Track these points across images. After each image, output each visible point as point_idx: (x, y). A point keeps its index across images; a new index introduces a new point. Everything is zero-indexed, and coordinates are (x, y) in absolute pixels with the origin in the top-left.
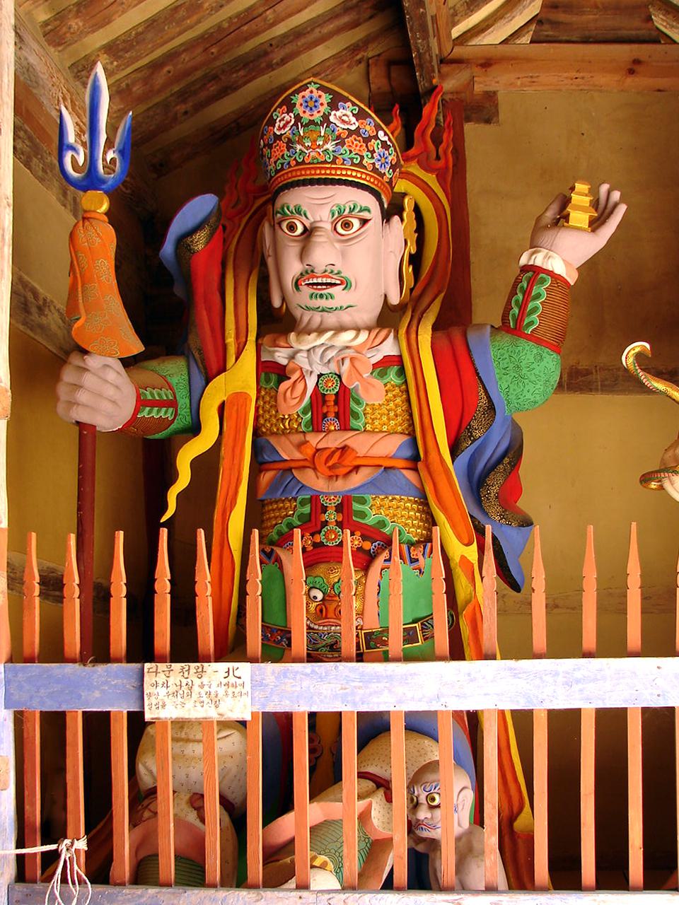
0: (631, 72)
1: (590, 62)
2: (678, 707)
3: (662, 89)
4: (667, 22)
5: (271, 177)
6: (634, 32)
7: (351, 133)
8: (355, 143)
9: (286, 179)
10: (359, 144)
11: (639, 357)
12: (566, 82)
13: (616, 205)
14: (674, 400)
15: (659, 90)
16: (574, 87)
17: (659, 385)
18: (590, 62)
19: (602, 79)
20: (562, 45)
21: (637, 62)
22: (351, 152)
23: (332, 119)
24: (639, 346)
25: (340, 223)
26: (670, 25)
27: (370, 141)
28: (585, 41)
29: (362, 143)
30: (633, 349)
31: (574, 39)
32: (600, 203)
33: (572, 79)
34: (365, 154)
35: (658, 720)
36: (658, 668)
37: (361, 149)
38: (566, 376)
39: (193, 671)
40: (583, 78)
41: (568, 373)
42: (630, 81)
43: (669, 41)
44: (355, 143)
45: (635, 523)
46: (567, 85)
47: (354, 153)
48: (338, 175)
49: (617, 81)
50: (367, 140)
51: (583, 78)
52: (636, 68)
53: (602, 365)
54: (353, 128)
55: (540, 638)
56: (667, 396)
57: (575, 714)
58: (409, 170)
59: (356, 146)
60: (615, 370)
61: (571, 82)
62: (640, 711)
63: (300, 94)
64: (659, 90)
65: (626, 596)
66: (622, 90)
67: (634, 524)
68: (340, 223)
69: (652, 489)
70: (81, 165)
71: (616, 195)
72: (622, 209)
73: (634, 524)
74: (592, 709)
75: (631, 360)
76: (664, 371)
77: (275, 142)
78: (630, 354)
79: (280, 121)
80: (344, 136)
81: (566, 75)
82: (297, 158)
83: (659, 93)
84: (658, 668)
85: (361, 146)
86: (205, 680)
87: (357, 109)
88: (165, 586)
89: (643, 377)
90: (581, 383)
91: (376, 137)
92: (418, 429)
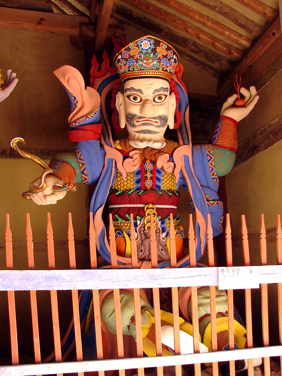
0: (39, 23)
1: (20, 17)
2: (281, 283)
3: (54, 32)
4: (60, 4)
5: (125, 72)
6: (42, 7)
11: (19, 143)
12: (10, 25)
13: (14, 79)
14: (36, 162)
15: (53, 33)
16: (13, 28)
17: (29, 156)
18: (20, 17)
19: (26, 25)
20: (8, 9)
21: (42, 19)
24: (18, 139)
26: (62, 6)
27: (171, 60)
28: (19, 8)
29: (167, 61)
30: (15, 140)
31: (14, 6)
32: (8, 77)
33: (12, 24)
35: (273, 288)
37: (167, 63)
38: (8, 151)
40: (17, 24)
41: (9, 150)
42: (39, 27)
43: (64, 13)
46: (10, 26)
47: (164, 66)
48: (153, 74)
49: (33, 27)
50: (169, 60)
51: (17, 24)
52: (42, 22)
53: (25, 147)
55: (31, 261)
56: (33, 161)
57: (69, 292)
58: (93, 66)
60: (31, 149)
61: (12, 25)
62: (267, 286)
64: (53, 33)
65: (47, 244)
66: (36, 31)
67: (70, 214)
69: (28, 199)
71: (14, 75)
72: (16, 81)
73: (70, 214)
74: (138, 289)
75: (15, 145)
76: (53, 150)
77: (129, 58)
78: (14, 142)
80: (161, 58)
81: (10, 22)
83: (53, 34)
85: (167, 62)
87: (167, 46)
89: (21, 152)
90: (15, 154)
91: (173, 58)
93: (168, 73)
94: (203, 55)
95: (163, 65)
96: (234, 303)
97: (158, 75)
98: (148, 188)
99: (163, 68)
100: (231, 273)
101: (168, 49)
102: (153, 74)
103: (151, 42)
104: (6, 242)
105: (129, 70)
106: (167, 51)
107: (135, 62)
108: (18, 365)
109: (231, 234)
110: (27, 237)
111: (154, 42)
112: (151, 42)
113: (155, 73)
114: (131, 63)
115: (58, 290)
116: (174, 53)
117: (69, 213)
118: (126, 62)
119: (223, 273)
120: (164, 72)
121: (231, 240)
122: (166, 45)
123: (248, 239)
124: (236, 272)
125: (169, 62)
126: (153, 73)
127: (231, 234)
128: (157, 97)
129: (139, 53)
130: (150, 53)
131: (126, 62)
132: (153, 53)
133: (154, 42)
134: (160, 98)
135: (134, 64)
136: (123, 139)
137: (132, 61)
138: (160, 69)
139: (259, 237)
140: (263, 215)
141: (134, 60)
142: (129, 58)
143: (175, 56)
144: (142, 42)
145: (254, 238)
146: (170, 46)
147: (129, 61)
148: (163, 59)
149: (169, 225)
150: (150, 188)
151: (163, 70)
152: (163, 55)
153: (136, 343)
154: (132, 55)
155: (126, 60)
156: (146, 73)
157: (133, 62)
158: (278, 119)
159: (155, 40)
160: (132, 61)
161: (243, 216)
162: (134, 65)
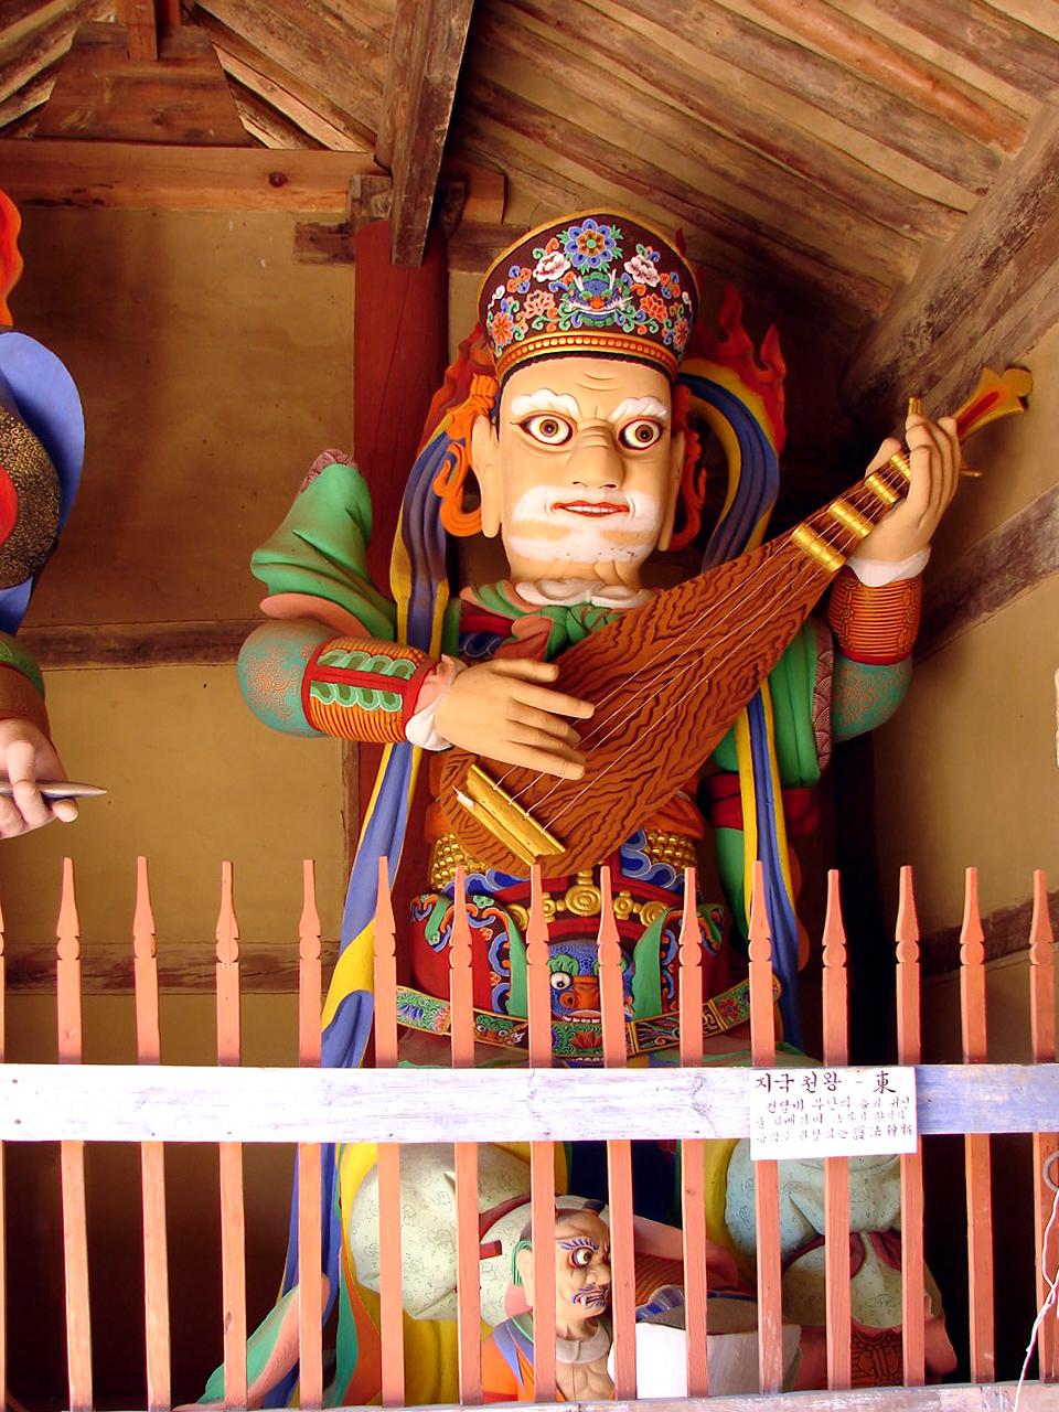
5: (514, 341)
7: (650, 290)
8: (654, 304)
9: (526, 354)
10: (659, 307)
22: (648, 318)
23: (627, 266)
25: (641, 423)
34: (665, 320)
36: (18, 1122)
39: (821, 1080)
44: (654, 304)
45: (837, 872)
54: (653, 284)
59: (655, 308)
62: (629, 1145)
63: (603, 226)
67: (833, 876)
68: (641, 423)
70: (773, 327)
73: (833, 876)
77: (531, 291)
79: (546, 262)
82: (538, 320)
84: (18, 1122)
85: (660, 309)
86: (840, 1094)
88: (905, 954)
91: (680, 300)
92: (768, 740)
93: (665, 351)
94: (326, 256)
96: (1033, 1197)
97: (540, 349)
100: (798, 1089)
103: (597, 234)
105: (531, 332)
110: (470, 959)
111: (621, 237)
112: (597, 234)
117: (305, 862)
119: (832, 1087)
121: (394, 958)
124: (821, 1087)
125: (668, 311)
129: (566, 272)
130: (606, 270)
132: (614, 271)
133: (621, 237)
134: (549, 428)
135: (548, 308)
136: (254, 571)
140: (1038, 871)
143: (685, 295)
145: (939, 956)
148: (645, 296)
155: (521, 298)
156: (554, 342)
157: (544, 302)
161: (68, 862)
162: (546, 311)
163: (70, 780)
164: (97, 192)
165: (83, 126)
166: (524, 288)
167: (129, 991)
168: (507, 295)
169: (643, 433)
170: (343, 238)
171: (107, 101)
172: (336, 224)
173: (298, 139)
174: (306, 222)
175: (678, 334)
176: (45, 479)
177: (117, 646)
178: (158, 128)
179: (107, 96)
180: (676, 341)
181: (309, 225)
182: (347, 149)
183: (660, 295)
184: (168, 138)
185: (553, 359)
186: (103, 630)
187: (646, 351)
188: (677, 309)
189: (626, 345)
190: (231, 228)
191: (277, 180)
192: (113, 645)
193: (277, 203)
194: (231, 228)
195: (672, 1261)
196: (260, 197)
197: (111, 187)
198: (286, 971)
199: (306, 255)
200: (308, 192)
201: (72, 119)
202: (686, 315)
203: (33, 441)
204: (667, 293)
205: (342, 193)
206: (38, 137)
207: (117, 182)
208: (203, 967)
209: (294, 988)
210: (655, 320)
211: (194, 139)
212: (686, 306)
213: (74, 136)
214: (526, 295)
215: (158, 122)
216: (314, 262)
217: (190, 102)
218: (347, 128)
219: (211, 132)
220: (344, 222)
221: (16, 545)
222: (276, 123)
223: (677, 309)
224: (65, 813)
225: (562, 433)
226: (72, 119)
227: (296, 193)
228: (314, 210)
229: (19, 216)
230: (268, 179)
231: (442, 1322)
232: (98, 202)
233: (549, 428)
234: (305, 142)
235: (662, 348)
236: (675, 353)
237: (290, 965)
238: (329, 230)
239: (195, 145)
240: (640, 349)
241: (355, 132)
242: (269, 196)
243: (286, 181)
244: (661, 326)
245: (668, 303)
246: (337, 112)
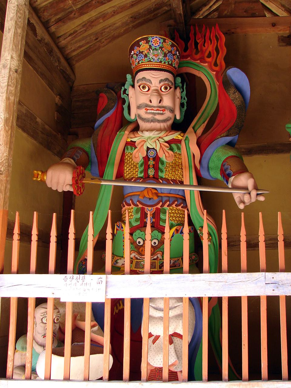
10: (171, 57)
67: (54, 214)
73: (54, 214)
77: (139, 54)
94: (285, 44)
95: (169, 59)
98: (151, 176)
99: (168, 62)
101: (172, 46)
102: (153, 66)
104: (107, 240)
106: (172, 47)
107: (143, 57)
108: (186, 382)
109: (32, 241)
113: (161, 66)
114: (140, 57)
115: (112, 298)
116: (177, 50)
118: (137, 57)
120: (169, 66)
122: (170, 42)
123: (165, 233)
126: (155, 65)
127: (32, 241)
128: (164, 86)
131: (137, 57)
137: (142, 56)
138: (166, 63)
139: (57, 243)
141: (143, 55)
142: (139, 54)
144: (153, 39)
146: (174, 43)
147: (139, 56)
149: (129, 218)
150: (152, 176)
151: (169, 64)
152: (168, 51)
153: (141, 372)
154: (141, 51)
155: (137, 55)
158: (56, 100)
159: (163, 39)
160: (142, 56)
163: (259, 189)
164: (233, 30)
165: (228, 14)
166: (138, 53)
167: (257, 249)
168: (134, 54)
169: (166, 88)
170: (289, 39)
171: (233, 7)
172: (287, 35)
173: (271, 14)
174: (280, 36)
175: (176, 63)
176: (243, 106)
177: (244, 151)
178: (245, 13)
179: (233, 6)
180: (176, 65)
181: (281, 36)
182: (285, 16)
183: (171, 53)
184: (246, 16)
185: (165, 72)
186: (241, 146)
187: (164, 67)
188: (175, 57)
189: (157, 66)
190: (263, 38)
191: (273, 25)
192: (243, 150)
193: (273, 31)
194: (263, 38)
195: (36, 299)
196: (270, 30)
197: (236, 29)
198: (287, 243)
199: (281, 44)
200: (281, 27)
201: (226, 12)
202: (178, 58)
203: (240, 96)
204: (173, 53)
205: (288, 27)
206: (219, 17)
207: (237, 28)
208: (268, 242)
209: (289, 247)
210: (170, 60)
211: (253, 16)
212: (178, 56)
213: (226, 17)
214: (138, 54)
215: (245, 12)
216: (283, 46)
217: (252, 6)
218: (285, 10)
219: (257, 13)
220: (289, 35)
221: (236, 124)
222: (266, 10)
223: (175, 57)
224: (262, 199)
225: (147, 89)
226: (226, 12)
227: (278, 28)
228: (282, 32)
229: (224, 37)
230: (271, 25)
231: (176, 331)
232: (233, 33)
233: (144, 87)
234: (273, 14)
235: (172, 67)
236: (176, 68)
237: (288, 240)
238: (285, 37)
239: (254, 17)
240: (168, 68)
241: (287, 11)
242: (272, 29)
243: (276, 25)
244: (172, 61)
245: (174, 55)
246: (283, 6)
